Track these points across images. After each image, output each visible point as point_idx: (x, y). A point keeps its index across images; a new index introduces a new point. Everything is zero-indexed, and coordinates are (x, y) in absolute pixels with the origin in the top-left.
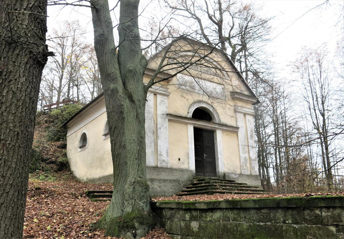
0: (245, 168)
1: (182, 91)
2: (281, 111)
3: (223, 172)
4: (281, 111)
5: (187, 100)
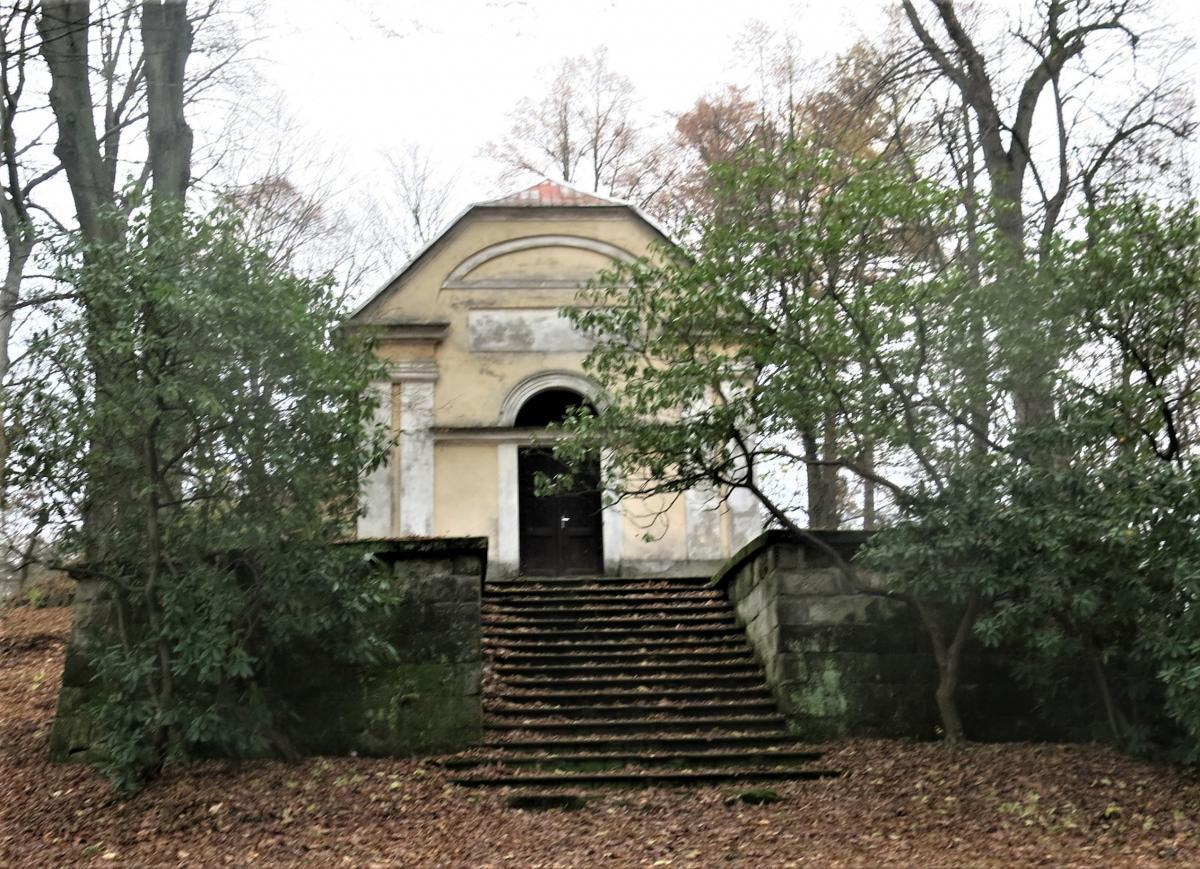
0: (702, 540)
1: (485, 358)
2: (944, 113)
3: (617, 558)
4: (944, 113)
5: (501, 378)
